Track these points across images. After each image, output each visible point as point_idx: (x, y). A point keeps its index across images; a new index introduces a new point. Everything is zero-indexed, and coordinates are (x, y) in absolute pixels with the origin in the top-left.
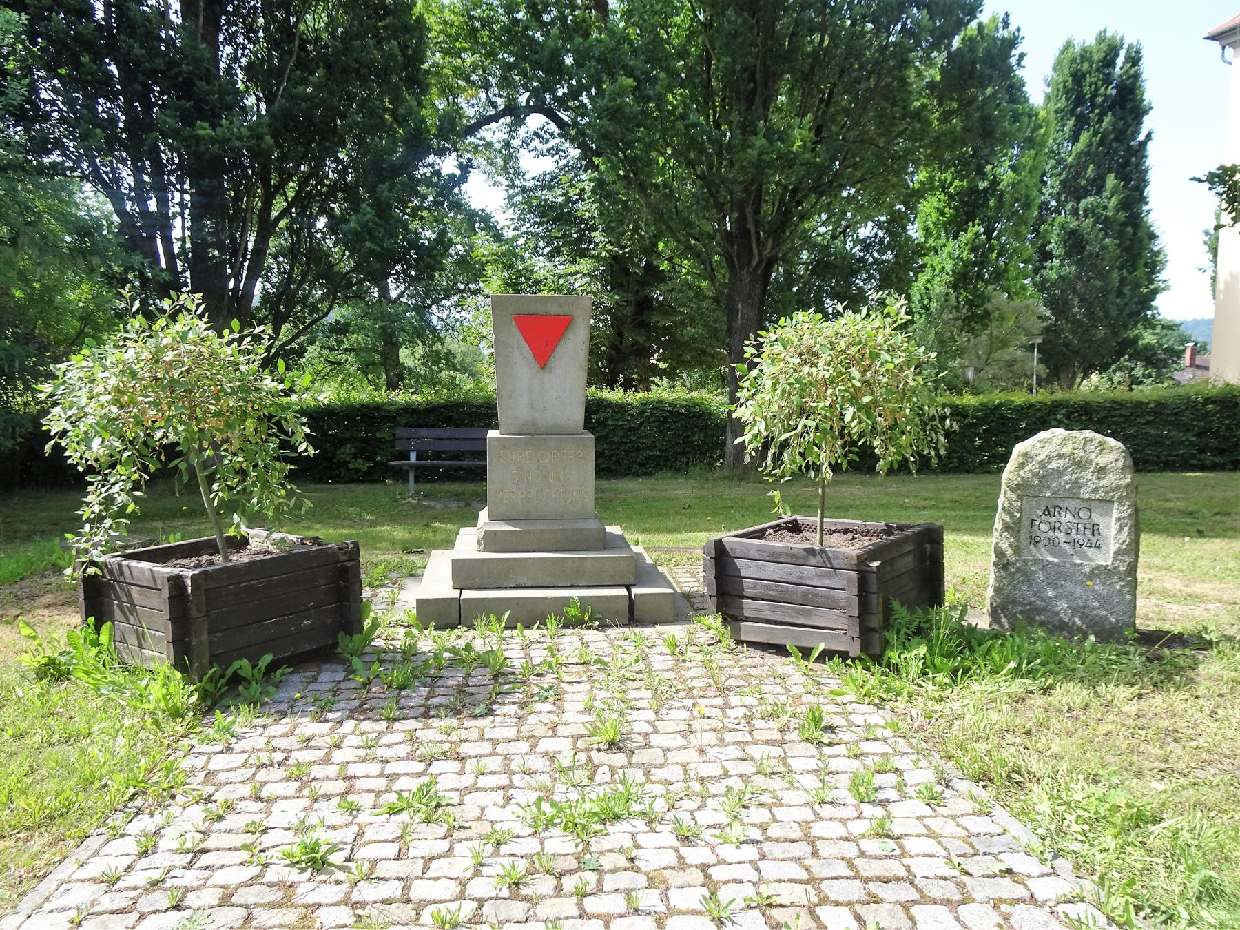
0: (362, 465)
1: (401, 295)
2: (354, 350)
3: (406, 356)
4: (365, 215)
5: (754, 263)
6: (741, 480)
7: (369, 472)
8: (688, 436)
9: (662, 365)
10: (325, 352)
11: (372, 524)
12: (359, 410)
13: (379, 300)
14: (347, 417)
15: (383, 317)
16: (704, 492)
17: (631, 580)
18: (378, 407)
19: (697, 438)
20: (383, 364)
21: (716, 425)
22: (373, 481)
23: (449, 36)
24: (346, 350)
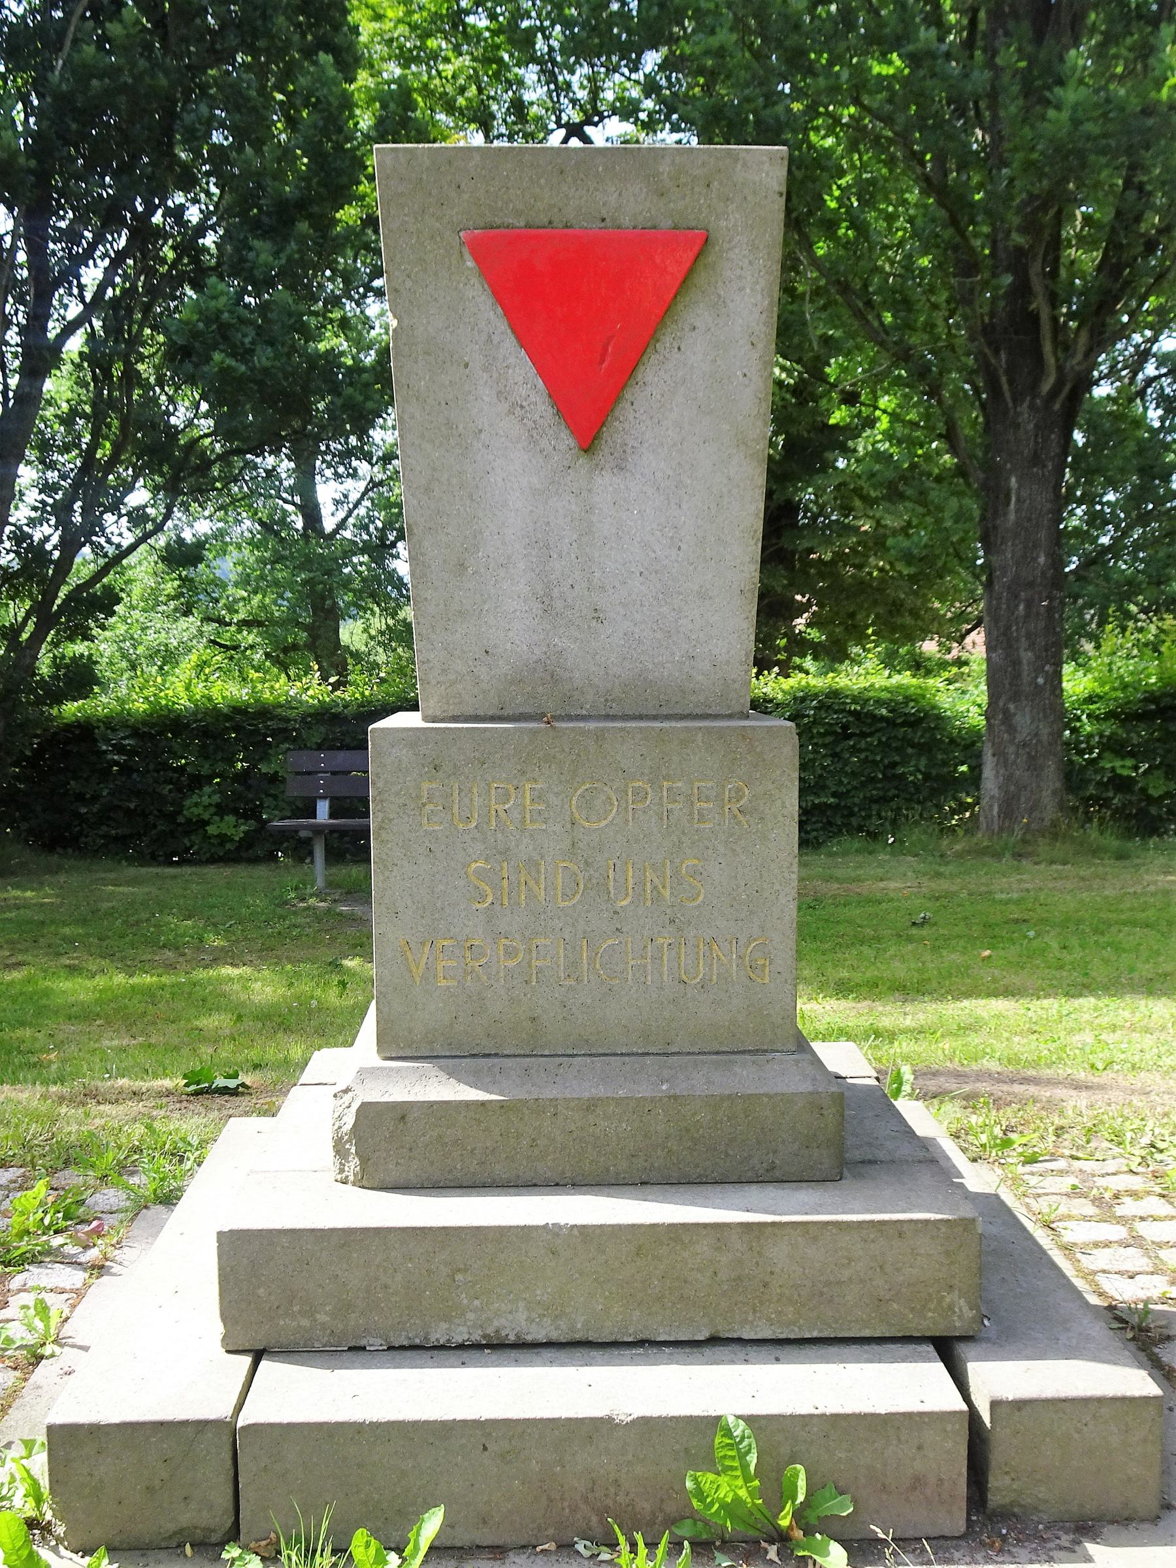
0: (233, 828)
1: (342, 525)
2: (260, 624)
3: (351, 633)
4: (214, 297)
5: (1046, 386)
6: (1018, 856)
7: (248, 842)
8: (894, 765)
9: (814, 634)
10: (209, 628)
11: (218, 958)
12: (227, 717)
13: (305, 536)
14: (205, 733)
15: (307, 563)
16: (944, 885)
17: (961, 1317)
18: (264, 712)
19: (913, 770)
20: (311, 646)
21: (952, 741)
22: (254, 861)
23: (413, 27)
24: (246, 624)
